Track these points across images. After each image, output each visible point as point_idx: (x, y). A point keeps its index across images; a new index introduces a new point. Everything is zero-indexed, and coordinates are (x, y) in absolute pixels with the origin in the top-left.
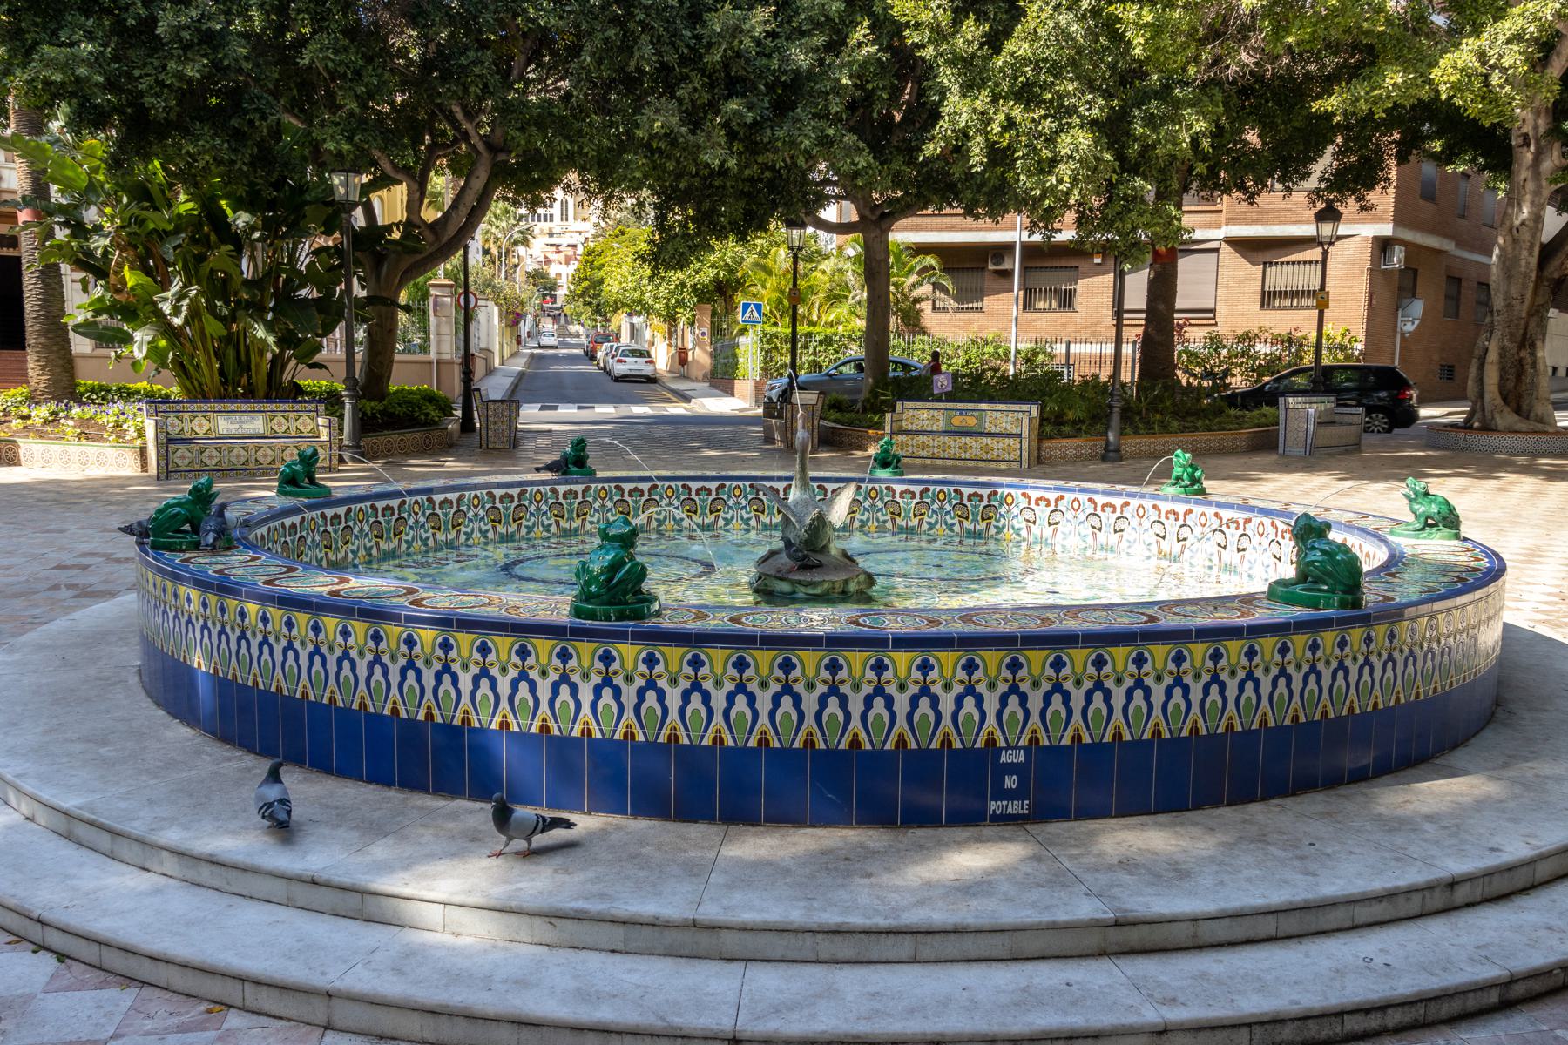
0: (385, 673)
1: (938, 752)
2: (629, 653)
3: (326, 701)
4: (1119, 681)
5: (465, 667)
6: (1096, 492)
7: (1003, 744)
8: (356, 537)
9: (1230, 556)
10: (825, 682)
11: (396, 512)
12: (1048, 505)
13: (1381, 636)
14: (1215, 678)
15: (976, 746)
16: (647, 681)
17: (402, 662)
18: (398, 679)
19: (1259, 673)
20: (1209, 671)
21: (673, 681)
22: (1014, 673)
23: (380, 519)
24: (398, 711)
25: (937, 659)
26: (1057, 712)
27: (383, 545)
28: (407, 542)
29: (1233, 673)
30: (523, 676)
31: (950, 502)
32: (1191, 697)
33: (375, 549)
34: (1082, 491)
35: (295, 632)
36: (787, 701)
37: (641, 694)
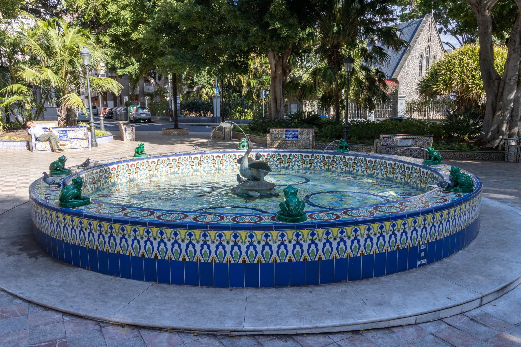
1: (272, 264)
2: (305, 233)
3: (105, 250)
4: (349, 238)
8: (103, 178)
10: (202, 240)
11: (116, 169)
12: (198, 159)
14: (369, 237)
17: (120, 236)
18: (119, 241)
19: (407, 230)
20: (367, 234)
22: (298, 237)
25: (164, 230)
26: (313, 250)
27: (96, 186)
28: (103, 184)
30: (148, 239)
31: (298, 158)
32: (373, 241)
33: (110, 182)
34: (231, 152)
35: (83, 225)
37: (202, 246)
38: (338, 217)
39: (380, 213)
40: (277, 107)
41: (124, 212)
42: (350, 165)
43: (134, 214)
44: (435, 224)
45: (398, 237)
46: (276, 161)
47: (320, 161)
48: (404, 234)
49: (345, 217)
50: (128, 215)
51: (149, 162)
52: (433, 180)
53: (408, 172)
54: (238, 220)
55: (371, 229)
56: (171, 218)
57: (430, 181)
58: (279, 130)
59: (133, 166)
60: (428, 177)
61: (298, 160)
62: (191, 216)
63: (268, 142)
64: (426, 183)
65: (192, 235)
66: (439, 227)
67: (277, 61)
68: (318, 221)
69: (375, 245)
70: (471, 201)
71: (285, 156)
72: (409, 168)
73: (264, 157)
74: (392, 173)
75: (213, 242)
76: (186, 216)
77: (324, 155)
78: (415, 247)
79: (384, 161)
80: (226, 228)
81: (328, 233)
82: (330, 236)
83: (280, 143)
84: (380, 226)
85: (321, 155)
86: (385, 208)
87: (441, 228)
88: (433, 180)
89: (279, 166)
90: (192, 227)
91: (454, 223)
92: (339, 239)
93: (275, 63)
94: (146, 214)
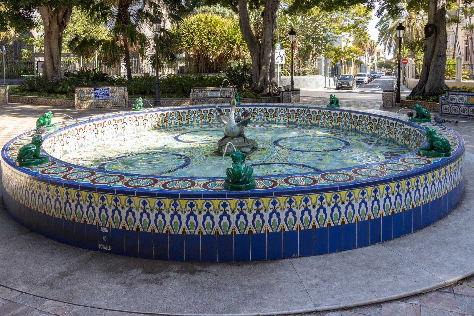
0: (81, 208)
2: (250, 202)
4: (298, 208)
5: (250, 211)
6: (289, 107)
7: (101, 225)
9: (100, 135)
13: (437, 174)
14: (350, 203)
15: (228, 234)
16: (174, 212)
17: (113, 207)
19: (379, 198)
21: (216, 212)
22: (274, 206)
23: (78, 133)
24: (75, 219)
29: (357, 201)
36: (225, 218)
37: (188, 217)
38: (315, 181)
39: (359, 177)
40: (53, 65)
41: (94, 177)
42: (335, 120)
43: (101, 180)
44: (420, 188)
45: (381, 203)
46: (263, 115)
47: (306, 115)
48: (376, 202)
49: (323, 181)
50: (96, 181)
51: (136, 117)
52: (416, 138)
53: (375, 124)
54: (209, 187)
55: (352, 195)
56: (139, 185)
57: (413, 138)
58: (86, 89)
59: (100, 125)
60: (411, 134)
61: (197, 115)
62: (161, 182)
63: (76, 103)
64: (410, 140)
65: (194, 205)
66: (424, 191)
67: (52, 16)
68: (295, 186)
69: (343, 215)
70: (457, 162)
71: (184, 113)
72: (393, 124)
73: (164, 116)
74: (377, 129)
75: (266, 210)
76: (156, 181)
77: (310, 110)
78: (389, 216)
79: (368, 116)
80: (198, 196)
81: (290, 202)
82: (293, 204)
83: (92, 103)
84: (348, 194)
85: (307, 109)
86: (365, 171)
87: (426, 192)
88: (416, 138)
89: (178, 124)
90: (162, 195)
91: (440, 186)
92: (302, 208)
93: (49, 18)
94: (114, 179)
